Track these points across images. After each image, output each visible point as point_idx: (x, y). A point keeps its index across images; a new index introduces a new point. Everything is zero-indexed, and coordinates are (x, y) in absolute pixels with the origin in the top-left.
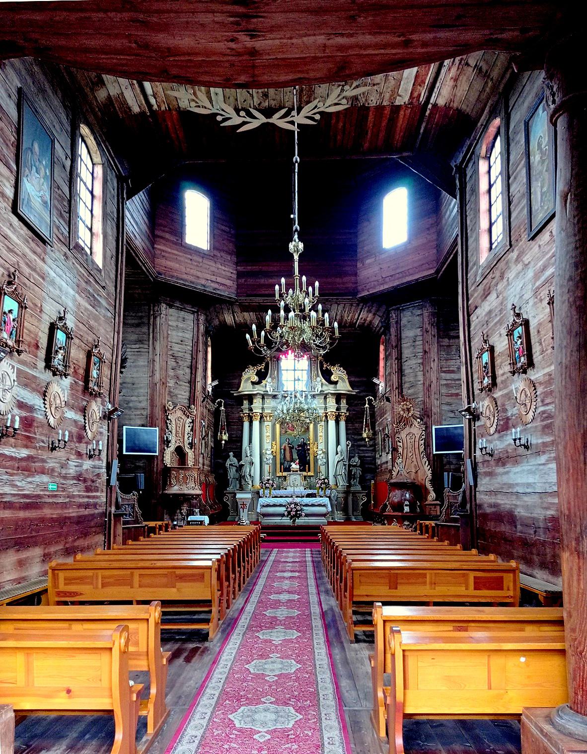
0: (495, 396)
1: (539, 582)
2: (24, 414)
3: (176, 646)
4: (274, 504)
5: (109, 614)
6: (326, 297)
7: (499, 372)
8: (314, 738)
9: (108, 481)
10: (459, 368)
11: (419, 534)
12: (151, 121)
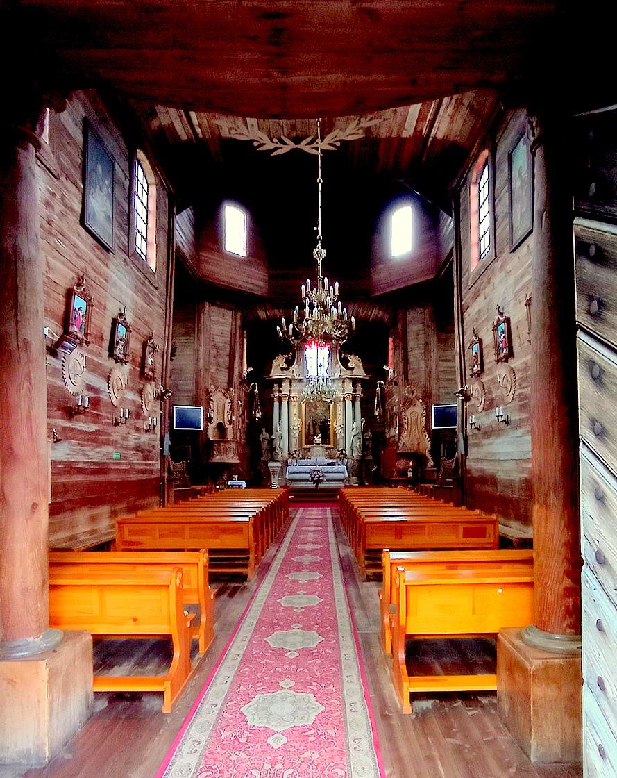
0: (483, 380)
1: (514, 530)
2: (92, 395)
3: (221, 585)
4: (300, 471)
5: (169, 559)
6: (345, 297)
7: (486, 361)
8: (334, 655)
9: (162, 451)
10: (454, 358)
11: (420, 495)
12: (196, 145)
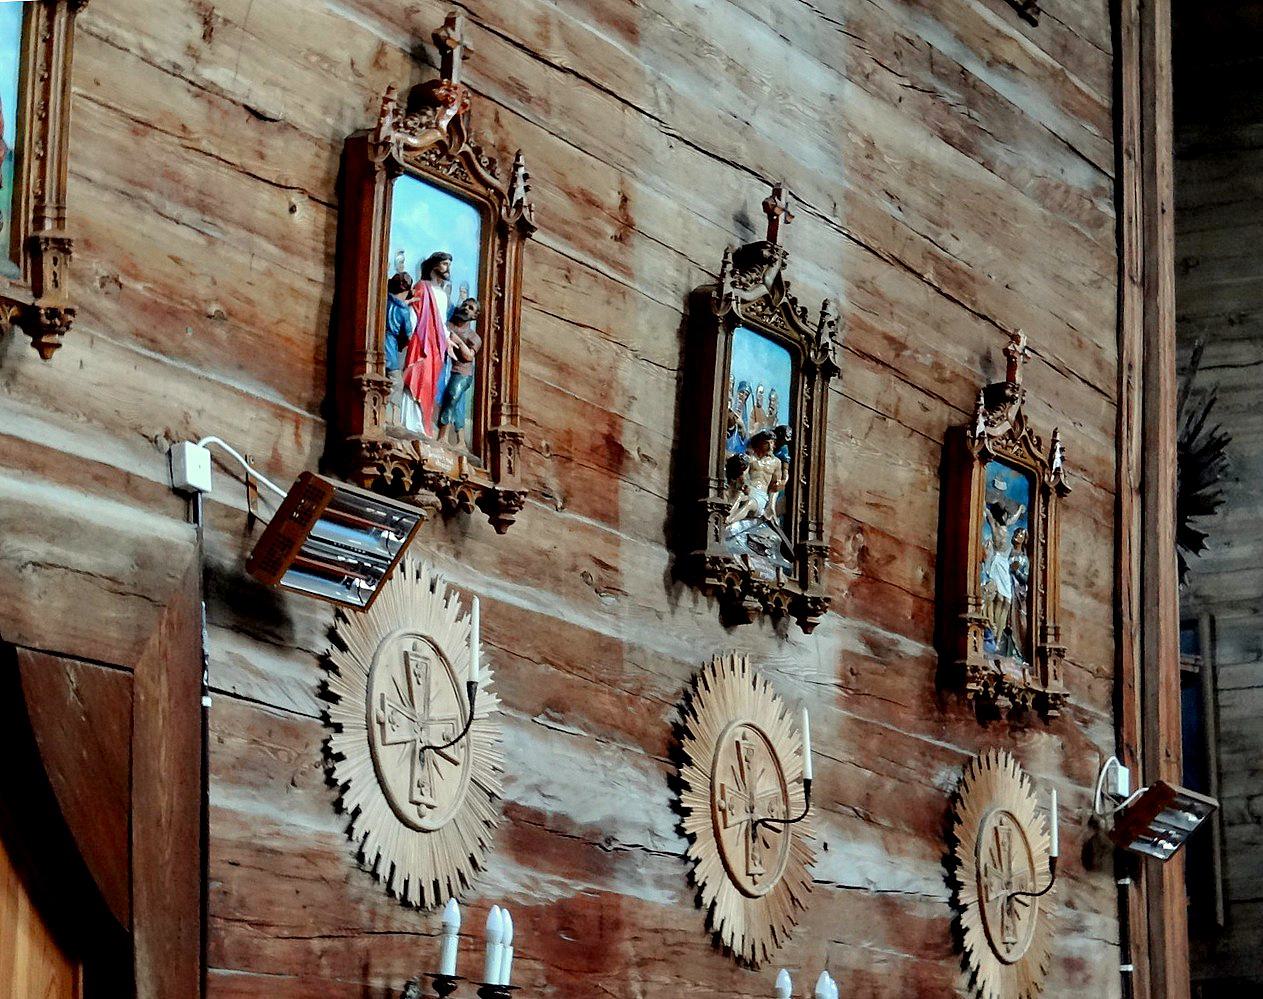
2: (550, 887)
